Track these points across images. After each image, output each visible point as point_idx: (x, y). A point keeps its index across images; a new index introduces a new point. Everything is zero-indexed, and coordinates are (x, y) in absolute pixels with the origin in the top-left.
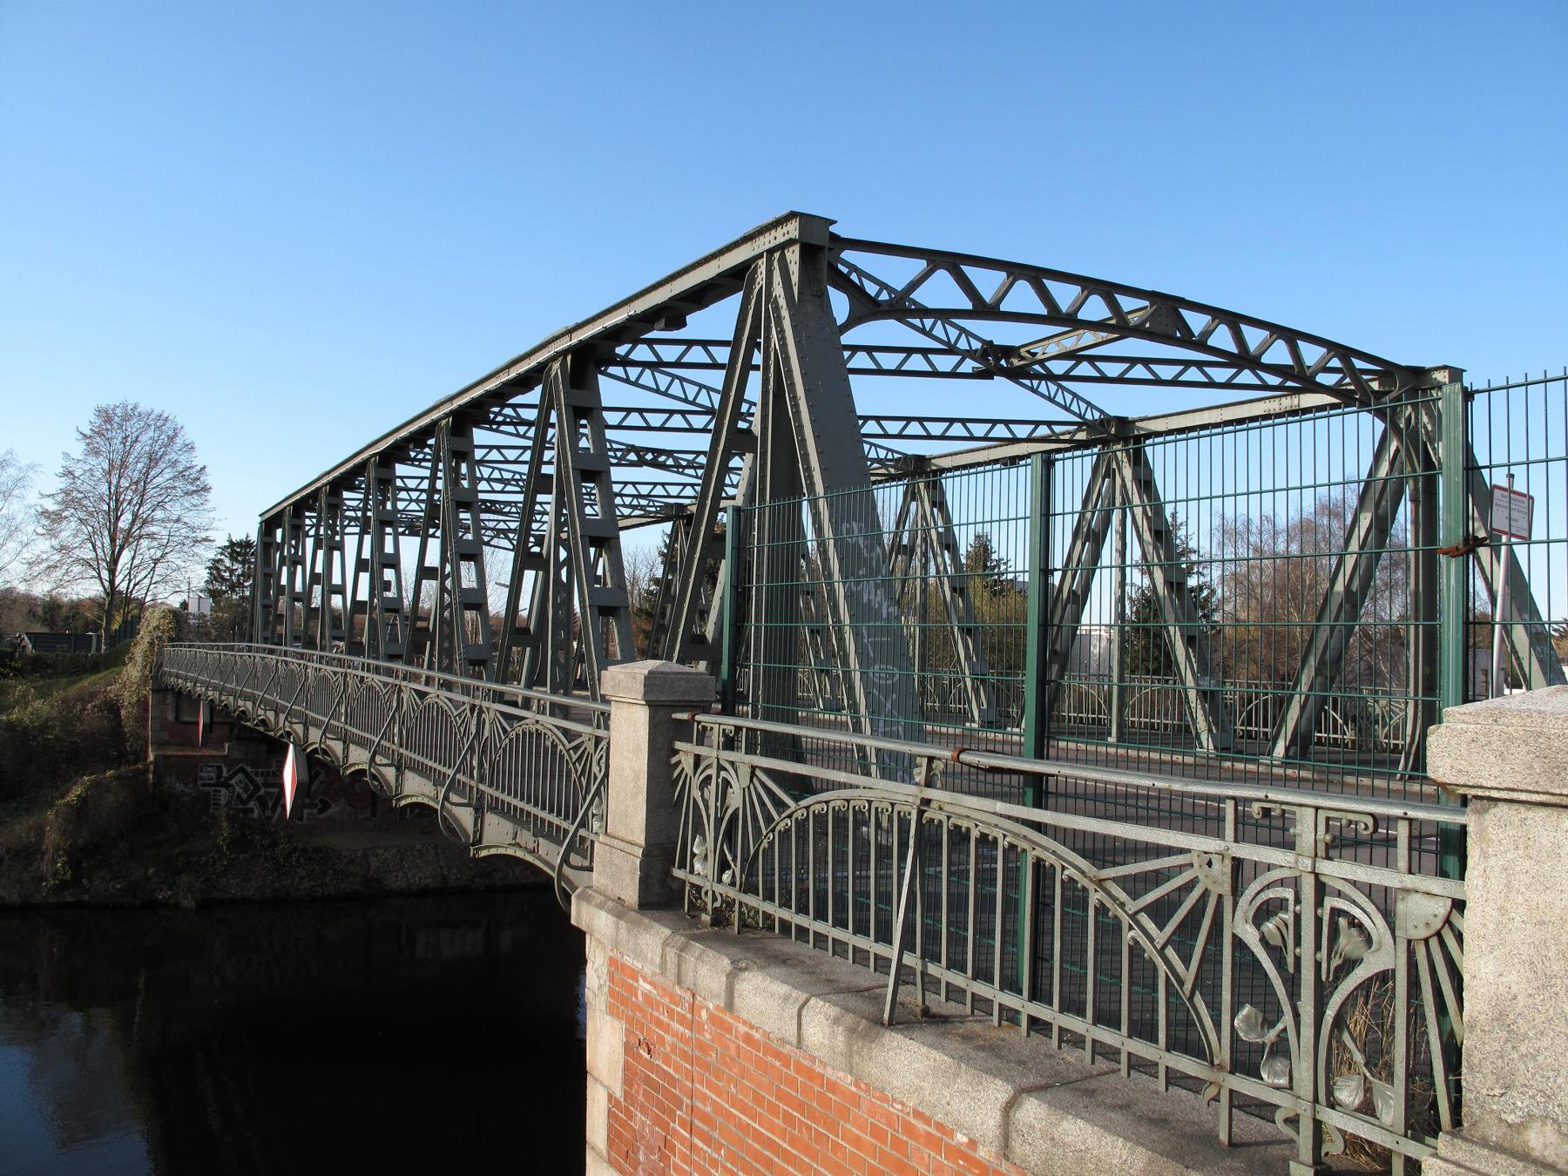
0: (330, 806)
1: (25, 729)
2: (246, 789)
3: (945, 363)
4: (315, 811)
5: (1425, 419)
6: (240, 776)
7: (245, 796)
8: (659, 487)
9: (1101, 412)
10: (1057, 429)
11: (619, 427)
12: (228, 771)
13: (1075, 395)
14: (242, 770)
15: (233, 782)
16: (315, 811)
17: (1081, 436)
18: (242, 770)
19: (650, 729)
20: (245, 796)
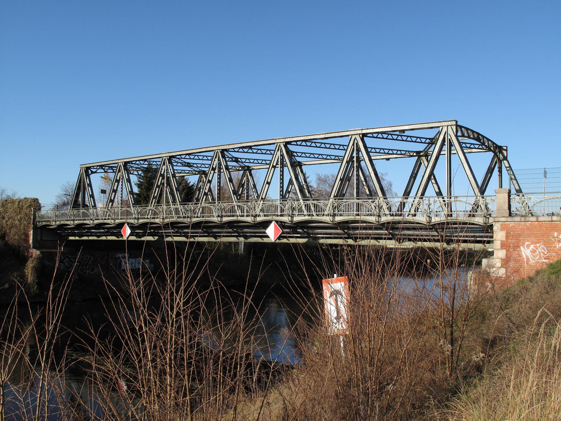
0: (94, 269)
1: (9, 245)
2: (69, 263)
3: (243, 160)
4: (90, 271)
5: (501, 156)
6: (67, 259)
7: (68, 266)
8: (308, 156)
9: (232, 155)
10: (340, 158)
11: (176, 166)
12: (63, 257)
13: (230, 154)
14: (68, 257)
15: (65, 261)
16: (90, 271)
17: (240, 169)
18: (68, 257)
19: (181, 241)
20: (68, 266)
